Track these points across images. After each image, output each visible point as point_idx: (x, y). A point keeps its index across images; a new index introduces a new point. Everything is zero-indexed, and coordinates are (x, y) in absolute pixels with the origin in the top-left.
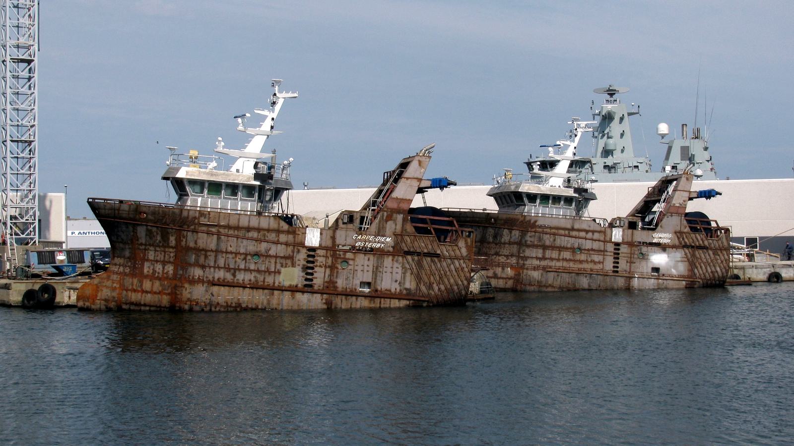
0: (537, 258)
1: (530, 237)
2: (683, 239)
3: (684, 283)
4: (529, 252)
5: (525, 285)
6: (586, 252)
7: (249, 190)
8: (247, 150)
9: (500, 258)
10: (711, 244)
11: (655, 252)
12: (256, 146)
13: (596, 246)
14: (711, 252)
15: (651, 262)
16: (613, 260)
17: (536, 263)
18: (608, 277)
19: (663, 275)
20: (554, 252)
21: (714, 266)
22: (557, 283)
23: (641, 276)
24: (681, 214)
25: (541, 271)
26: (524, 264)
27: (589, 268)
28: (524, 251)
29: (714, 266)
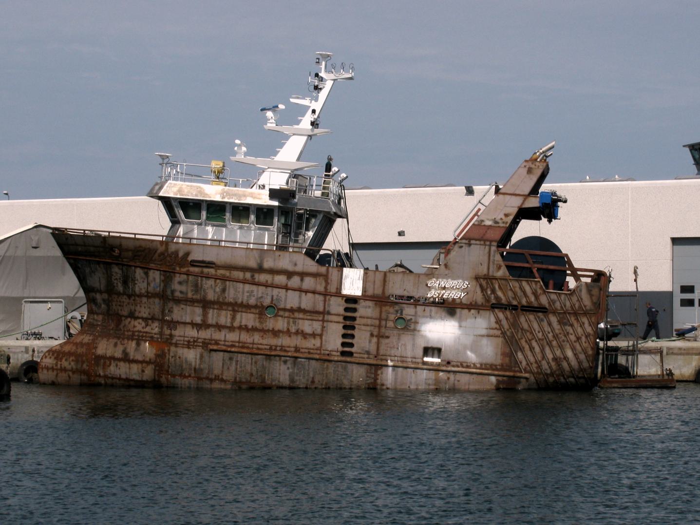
0: (193, 325)
1: (180, 283)
2: (493, 291)
3: (493, 379)
4: (181, 313)
5: (174, 376)
6: (287, 314)
7: (263, 215)
8: (278, 158)
9: (136, 323)
10: (554, 302)
11: (431, 317)
12: (291, 151)
13: (307, 301)
14: (554, 319)
15: (424, 337)
16: (343, 331)
17: (192, 333)
18: (331, 365)
19: (449, 363)
20: (224, 312)
21: (561, 347)
22: (229, 374)
23: (400, 364)
24: (491, 241)
25: (199, 350)
26: (171, 335)
27: (293, 345)
28: (171, 311)
29: (561, 347)
